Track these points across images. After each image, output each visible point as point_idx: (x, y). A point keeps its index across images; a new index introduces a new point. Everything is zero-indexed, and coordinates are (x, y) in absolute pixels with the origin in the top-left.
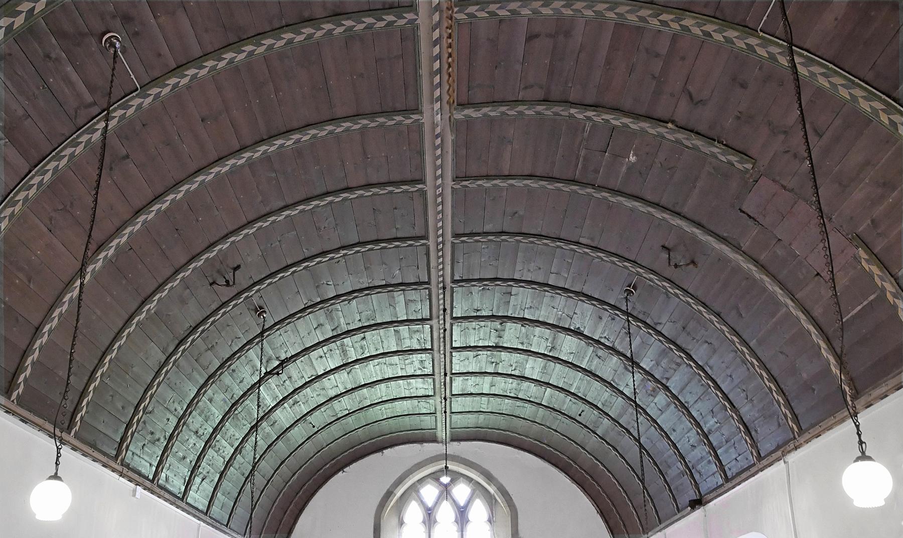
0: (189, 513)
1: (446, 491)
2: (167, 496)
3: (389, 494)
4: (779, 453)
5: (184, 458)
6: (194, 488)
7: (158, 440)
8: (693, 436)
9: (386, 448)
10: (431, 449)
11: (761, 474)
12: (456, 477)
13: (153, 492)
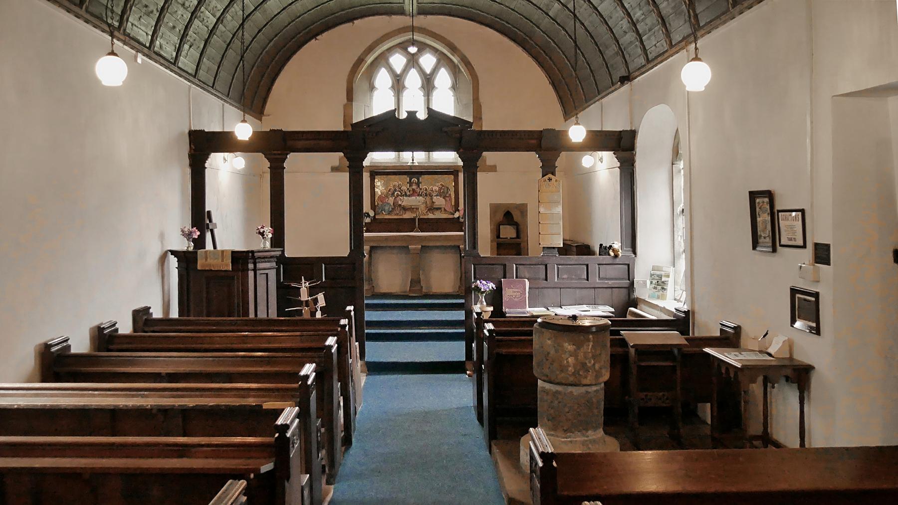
0: (181, 76)
1: (413, 61)
2: (162, 61)
3: (360, 61)
4: (683, 43)
5: (174, 27)
6: (184, 53)
7: (152, 12)
8: (625, 24)
9: (357, 19)
10: (398, 21)
11: (671, 58)
12: (422, 47)
13: (150, 58)
